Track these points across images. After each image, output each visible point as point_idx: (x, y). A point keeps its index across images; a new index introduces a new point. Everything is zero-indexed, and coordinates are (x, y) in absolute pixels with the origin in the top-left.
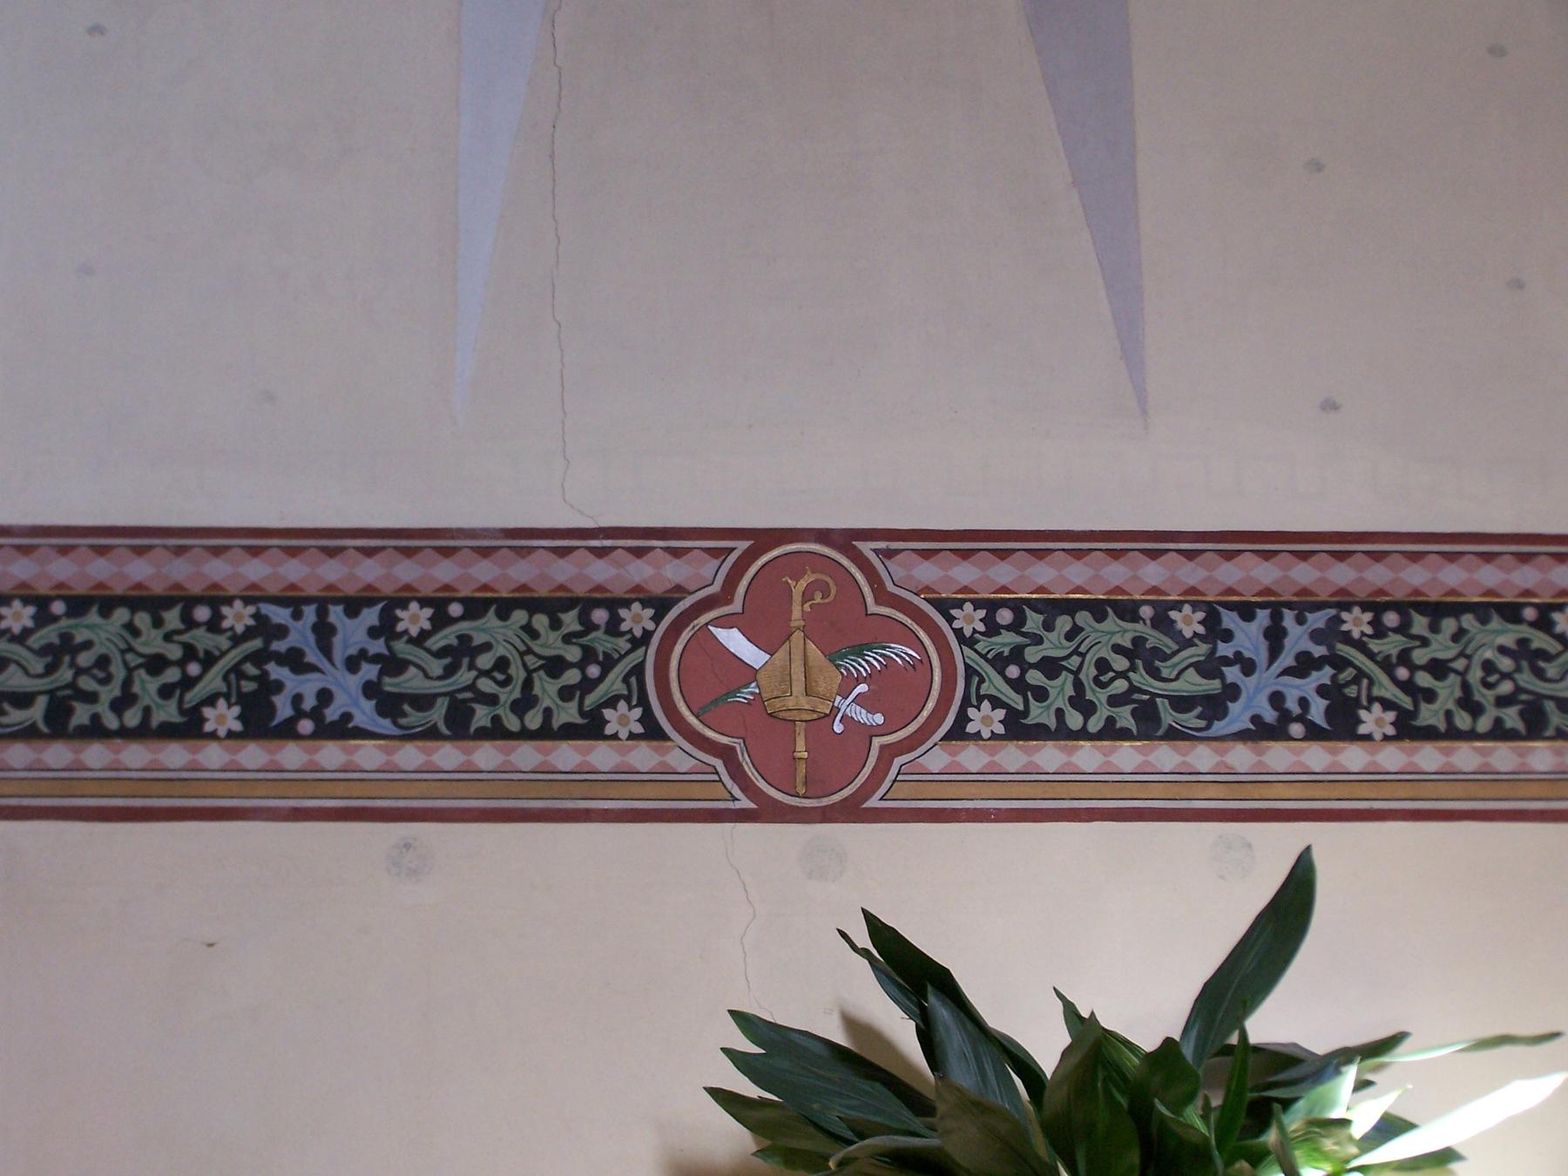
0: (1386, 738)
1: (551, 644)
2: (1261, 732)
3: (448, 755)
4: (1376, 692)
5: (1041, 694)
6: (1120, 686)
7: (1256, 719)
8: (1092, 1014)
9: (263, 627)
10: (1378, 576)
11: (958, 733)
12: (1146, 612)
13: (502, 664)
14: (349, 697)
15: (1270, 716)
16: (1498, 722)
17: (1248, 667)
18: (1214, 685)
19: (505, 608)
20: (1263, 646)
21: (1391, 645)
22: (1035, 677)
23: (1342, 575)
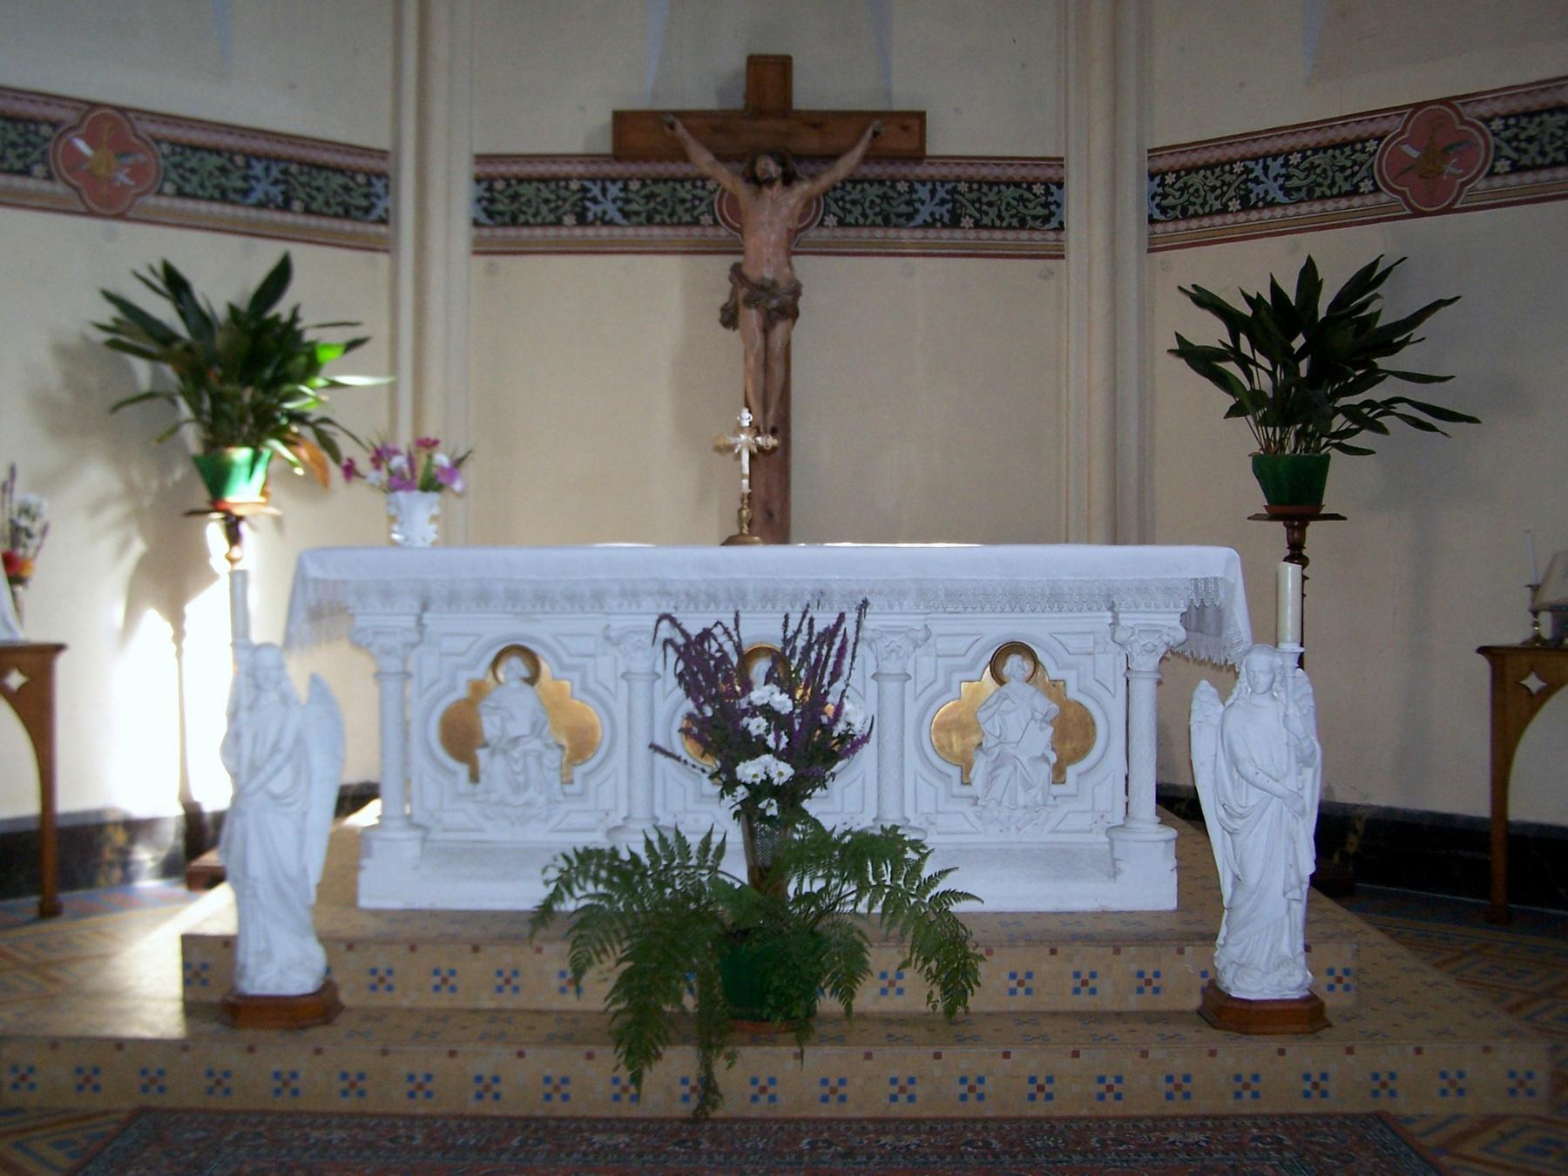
0: (970, 228)
1: (546, 194)
2: (261, 205)
3: (643, 232)
4: (968, 211)
5: (986, 213)
6: (1014, 211)
7: (925, 221)
8: (1258, 294)
9: (584, 190)
10: (971, 171)
11: (821, 224)
12: (888, 183)
13: (665, 201)
14: (613, 213)
15: (929, 220)
16: (874, 221)
17: (923, 203)
18: (1046, 212)
19: (666, 181)
20: (928, 195)
21: (974, 196)
22: (984, 208)
23: (957, 171)
